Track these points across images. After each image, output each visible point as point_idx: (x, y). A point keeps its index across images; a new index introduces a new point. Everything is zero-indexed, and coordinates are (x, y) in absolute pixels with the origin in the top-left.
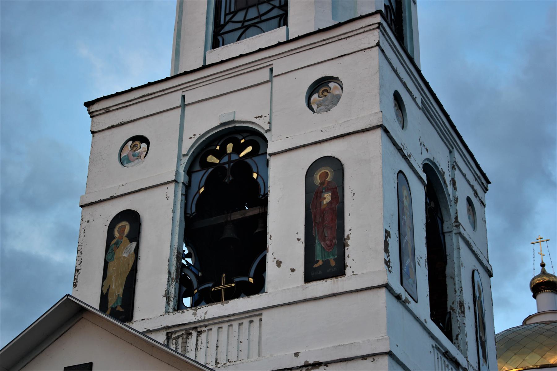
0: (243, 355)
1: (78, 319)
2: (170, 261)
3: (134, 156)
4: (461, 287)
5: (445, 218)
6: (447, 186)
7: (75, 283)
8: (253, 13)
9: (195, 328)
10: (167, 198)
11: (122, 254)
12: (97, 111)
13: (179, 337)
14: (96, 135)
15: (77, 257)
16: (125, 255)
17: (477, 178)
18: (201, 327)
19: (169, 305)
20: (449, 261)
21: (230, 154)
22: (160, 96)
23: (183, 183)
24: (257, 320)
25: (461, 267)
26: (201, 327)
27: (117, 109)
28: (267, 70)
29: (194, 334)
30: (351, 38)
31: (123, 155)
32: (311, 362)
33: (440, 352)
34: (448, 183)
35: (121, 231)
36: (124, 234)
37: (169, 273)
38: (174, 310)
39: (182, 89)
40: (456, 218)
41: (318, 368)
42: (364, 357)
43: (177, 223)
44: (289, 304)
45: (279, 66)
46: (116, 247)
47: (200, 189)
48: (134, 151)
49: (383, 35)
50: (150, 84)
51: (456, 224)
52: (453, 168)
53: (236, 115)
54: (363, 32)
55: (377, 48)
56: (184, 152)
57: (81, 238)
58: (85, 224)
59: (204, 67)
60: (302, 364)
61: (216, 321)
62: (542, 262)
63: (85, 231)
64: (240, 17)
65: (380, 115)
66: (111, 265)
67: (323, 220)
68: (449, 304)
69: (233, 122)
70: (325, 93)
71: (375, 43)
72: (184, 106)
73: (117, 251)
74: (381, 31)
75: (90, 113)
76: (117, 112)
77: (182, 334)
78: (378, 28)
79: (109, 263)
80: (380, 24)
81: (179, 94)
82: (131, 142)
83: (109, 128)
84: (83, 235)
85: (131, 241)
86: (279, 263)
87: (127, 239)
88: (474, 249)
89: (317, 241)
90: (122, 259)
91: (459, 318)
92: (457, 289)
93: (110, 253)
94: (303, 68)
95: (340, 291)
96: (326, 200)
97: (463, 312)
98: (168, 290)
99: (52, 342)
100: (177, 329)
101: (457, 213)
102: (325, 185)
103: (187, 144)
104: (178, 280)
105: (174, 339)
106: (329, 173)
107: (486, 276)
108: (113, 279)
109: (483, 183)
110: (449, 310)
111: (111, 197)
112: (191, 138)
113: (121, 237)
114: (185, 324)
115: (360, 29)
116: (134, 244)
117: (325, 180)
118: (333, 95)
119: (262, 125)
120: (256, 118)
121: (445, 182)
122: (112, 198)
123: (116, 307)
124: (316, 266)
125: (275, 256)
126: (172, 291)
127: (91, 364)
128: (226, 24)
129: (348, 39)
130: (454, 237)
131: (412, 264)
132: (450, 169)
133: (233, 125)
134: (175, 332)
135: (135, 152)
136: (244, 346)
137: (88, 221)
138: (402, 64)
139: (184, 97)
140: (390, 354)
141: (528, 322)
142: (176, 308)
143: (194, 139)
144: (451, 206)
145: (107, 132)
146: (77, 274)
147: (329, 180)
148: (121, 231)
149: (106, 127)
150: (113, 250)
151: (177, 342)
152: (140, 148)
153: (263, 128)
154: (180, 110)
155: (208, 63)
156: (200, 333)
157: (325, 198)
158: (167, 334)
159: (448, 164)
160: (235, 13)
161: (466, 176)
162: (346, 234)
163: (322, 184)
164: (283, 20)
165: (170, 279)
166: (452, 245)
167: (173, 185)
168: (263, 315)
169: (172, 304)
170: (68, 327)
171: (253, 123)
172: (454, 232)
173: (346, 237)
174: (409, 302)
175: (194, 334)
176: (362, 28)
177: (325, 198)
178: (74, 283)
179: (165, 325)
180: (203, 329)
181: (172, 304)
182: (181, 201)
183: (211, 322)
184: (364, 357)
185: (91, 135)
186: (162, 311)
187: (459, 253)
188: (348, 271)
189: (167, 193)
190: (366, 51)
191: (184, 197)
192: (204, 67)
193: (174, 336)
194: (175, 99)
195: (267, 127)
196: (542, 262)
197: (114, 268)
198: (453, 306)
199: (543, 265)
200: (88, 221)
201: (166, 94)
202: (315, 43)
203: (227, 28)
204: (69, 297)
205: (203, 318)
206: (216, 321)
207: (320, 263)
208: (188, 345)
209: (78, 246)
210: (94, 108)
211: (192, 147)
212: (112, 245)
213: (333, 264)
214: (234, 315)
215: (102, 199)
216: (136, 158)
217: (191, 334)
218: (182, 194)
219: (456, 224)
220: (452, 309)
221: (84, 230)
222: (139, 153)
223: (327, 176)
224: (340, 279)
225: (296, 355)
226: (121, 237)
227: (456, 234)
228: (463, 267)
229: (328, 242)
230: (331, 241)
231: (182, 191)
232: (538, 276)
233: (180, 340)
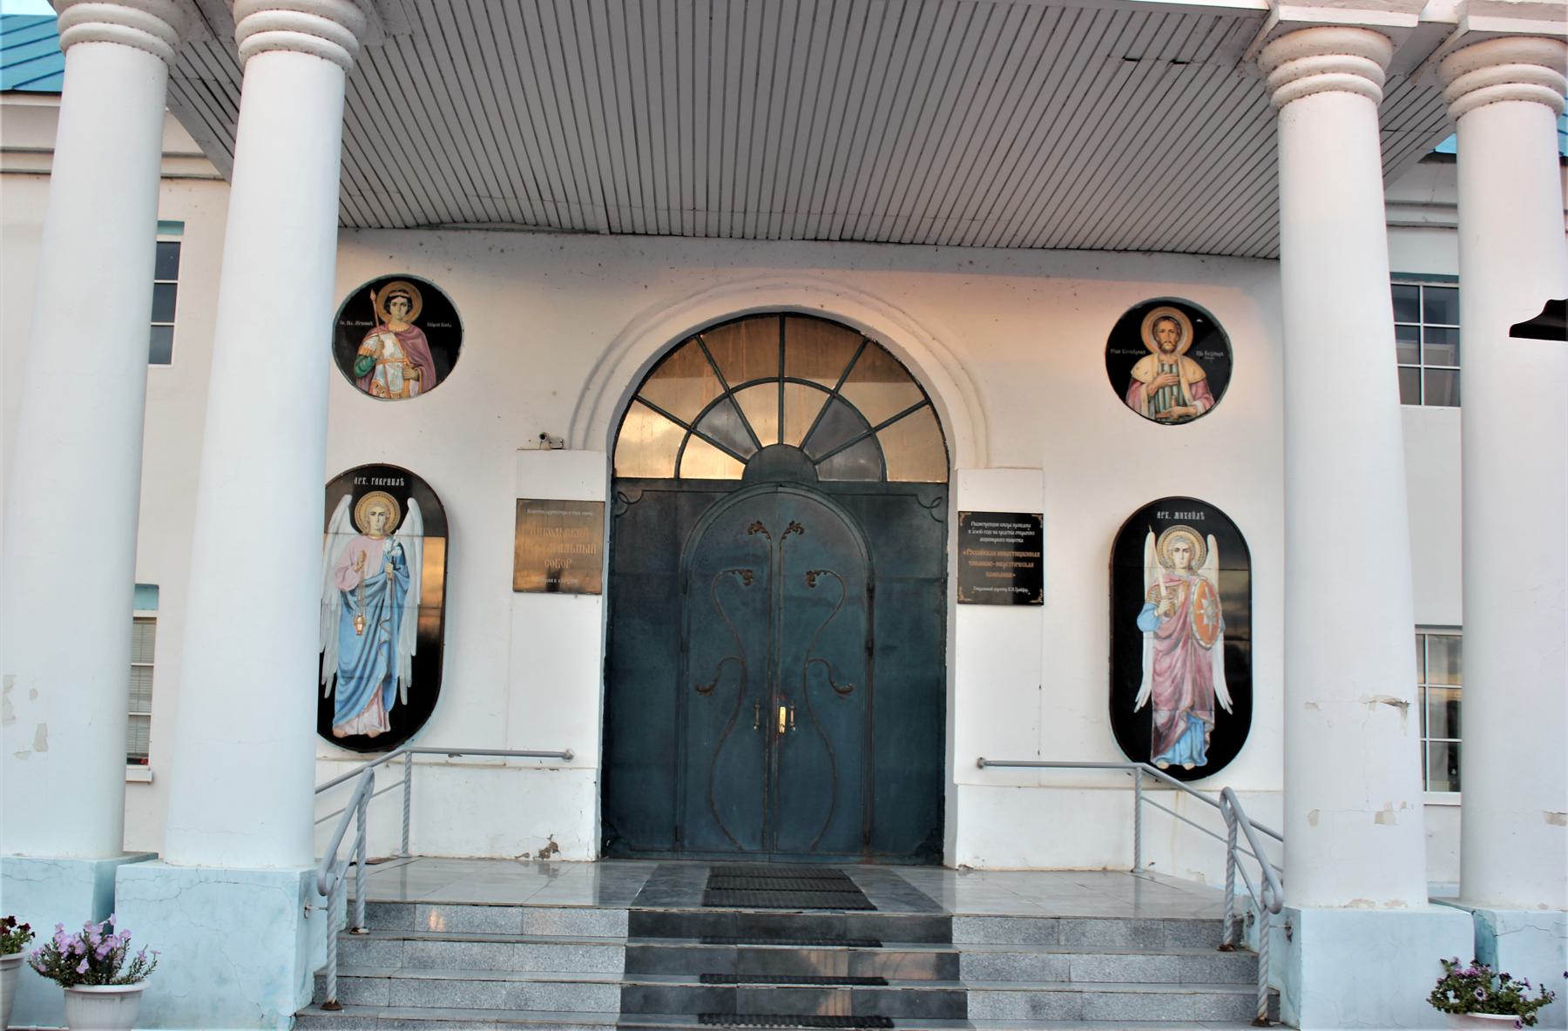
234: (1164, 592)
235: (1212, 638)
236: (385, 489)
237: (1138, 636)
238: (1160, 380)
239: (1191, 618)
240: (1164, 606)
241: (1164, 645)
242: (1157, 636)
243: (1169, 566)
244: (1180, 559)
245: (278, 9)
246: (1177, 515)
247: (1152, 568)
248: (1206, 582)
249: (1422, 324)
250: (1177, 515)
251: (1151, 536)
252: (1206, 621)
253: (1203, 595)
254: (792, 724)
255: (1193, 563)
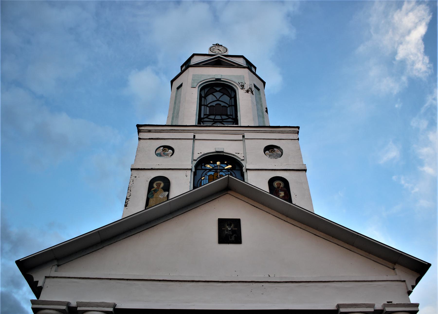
1: (225, 193)
7: (126, 205)
8: (218, 117)
10: (187, 176)
11: (159, 195)
15: (298, 139)
22: (181, 132)
27: (155, 132)
30: (284, 134)
35: (159, 185)
36: (160, 187)
39: (194, 132)
45: (247, 135)
46: (155, 192)
48: (164, 152)
54: (290, 133)
57: (131, 184)
63: (133, 181)
69: (223, 152)
73: (155, 194)
76: (155, 133)
79: (150, 199)
82: (162, 148)
83: (150, 139)
84: (132, 183)
87: (162, 189)
90: (159, 198)
93: (150, 194)
94: (260, 139)
96: (282, 195)
99: (205, 203)
106: (282, 184)
111: (151, 168)
112: (199, 154)
115: (289, 131)
116: (167, 193)
117: (280, 186)
118: (277, 153)
119: (240, 156)
129: (283, 134)
133: (222, 154)
135: (165, 153)
137: (136, 177)
146: (127, 200)
147: (282, 187)
149: (148, 138)
150: (153, 193)
152: (168, 151)
153: (240, 158)
157: (281, 194)
170: (218, 196)
171: (234, 155)
176: (290, 131)
177: (281, 194)
178: (125, 204)
190: (292, 140)
194: (191, 136)
197: (153, 202)
201: (184, 132)
202: (267, 131)
209: (129, 187)
211: (199, 157)
212: (152, 191)
216: (165, 155)
221: (133, 181)
222: (167, 153)
223: (281, 185)
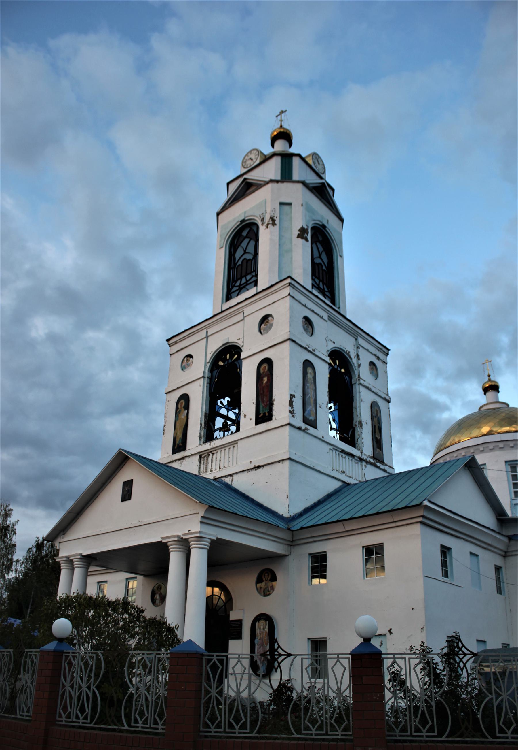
0: (230, 464)
2: (201, 418)
3: (187, 365)
4: (361, 413)
5: (353, 376)
6: (351, 359)
9: (211, 452)
10: (200, 386)
12: (172, 343)
13: (205, 456)
14: (172, 356)
16: (183, 417)
17: (379, 349)
18: (213, 451)
19: (201, 441)
20: (354, 400)
21: (228, 360)
23: (208, 377)
24: (235, 445)
25: (361, 402)
26: (213, 451)
28: (242, 313)
29: (211, 455)
31: (183, 365)
32: (256, 466)
33: (338, 451)
34: (352, 357)
35: (181, 405)
37: (201, 424)
38: (204, 443)
39: (206, 328)
40: (359, 375)
41: (260, 468)
42: (279, 462)
43: (205, 399)
44: (248, 437)
45: (247, 311)
47: (215, 379)
49: (293, 288)
50: (193, 327)
51: (359, 379)
52: (358, 348)
53: (230, 339)
55: (289, 297)
56: (208, 361)
58: (167, 402)
59: (222, 312)
60: (253, 467)
61: (219, 448)
62: (489, 374)
64: (238, 284)
65: (289, 333)
66: (177, 422)
67: (263, 392)
68: (354, 422)
69: (228, 343)
70: (267, 324)
71: (287, 294)
72: (207, 337)
74: (291, 287)
75: (169, 345)
77: (206, 455)
78: (289, 285)
80: (290, 284)
81: (205, 331)
85: (185, 410)
86: (245, 416)
88: (372, 390)
89: (261, 403)
91: (359, 430)
92: (358, 414)
95: (269, 428)
97: (361, 426)
98: (200, 433)
100: (203, 453)
101: (359, 373)
102: (265, 373)
103: (209, 356)
104: (206, 428)
105: (203, 458)
107: (386, 403)
108: (178, 429)
109: (384, 352)
110: (354, 426)
112: (210, 353)
113: (181, 408)
114: (206, 450)
119: (240, 343)
120: (238, 340)
121: (350, 357)
122: (178, 388)
123: (179, 444)
124: (260, 416)
125: (244, 412)
126: (202, 433)
127: (132, 480)
128: (233, 287)
130: (357, 386)
131: (314, 409)
132: (355, 349)
134: (203, 454)
136: (231, 459)
137: (169, 401)
138: (310, 300)
139: (207, 332)
140: (289, 459)
141: (481, 409)
142: (205, 442)
143: (212, 354)
144: (356, 369)
145: (176, 354)
148: (181, 405)
151: (204, 459)
153: (240, 345)
154: (205, 340)
155: (223, 310)
156: (213, 454)
158: (200, 455)
159: (353, 346)
160: (236, 282)
161: (369, 350)
162: (273, 398)
163: (263, 372)
164: (256, 283)
165: (202, 427)
166: (356, 391)
167: (202, 379)
168: (238, 443)
169: (202, 440)
172: (358, 383)
173: (273, 400)
174: (308, 430)
175: (211, 455)
179: (198, 451)
180: (215, 452)
181: (202, 440)
182: (207, 387)
183: (217, 448)
184: (279, 462)
185: (170, 356)
186: (198, 444)
187: (360, 394)
188: (274, 418)
189: (332, 341)
191: (208, 384)
192: (222, 312)
193: (203, 456)
194: (203, 334)
195: (242, 345)
196: (489, 374)
198: (356, 424)
199: (489, 376)
200: (169, 401)
203: (233, 290)
204: (121, 450)
205: (213, 447)
206: (219, 448)
207: (262, 414)
208: (208, 460)
210: (171, 342)
213: (267, 414)
214: (226, 444)
215: (170, 390)
217: (209, 455)
218: (207, 383)
219: (359, 379)
220: (356, 425)
224: (270, 422)
225: (251, 462)
226: (181, 408)
227: (358, 384)
228: (363, 402)
229: (265, 403)
230: (267, 403)
231: (207, 381)
232: (486, 383)
233: (205, 458)
234: (259, 635)
235: (267, 645)
236: (263, 619)
237: (255, 644)
238: (265, 587)
239: (264, 640)
240: (259, 638)
241: (259, 647)
242: (258, 645)
243: (260, 629)
244: (262, 627)
245: (389, 408)
246: (262, 617)
247: (257, 629)
248: (266, 632)
249: (319, 564)
250: (262, 617)
251: (257, 622)
252: (266, 640)
253: (265, 635)
254: (476, 691)
255: (264, 628)
